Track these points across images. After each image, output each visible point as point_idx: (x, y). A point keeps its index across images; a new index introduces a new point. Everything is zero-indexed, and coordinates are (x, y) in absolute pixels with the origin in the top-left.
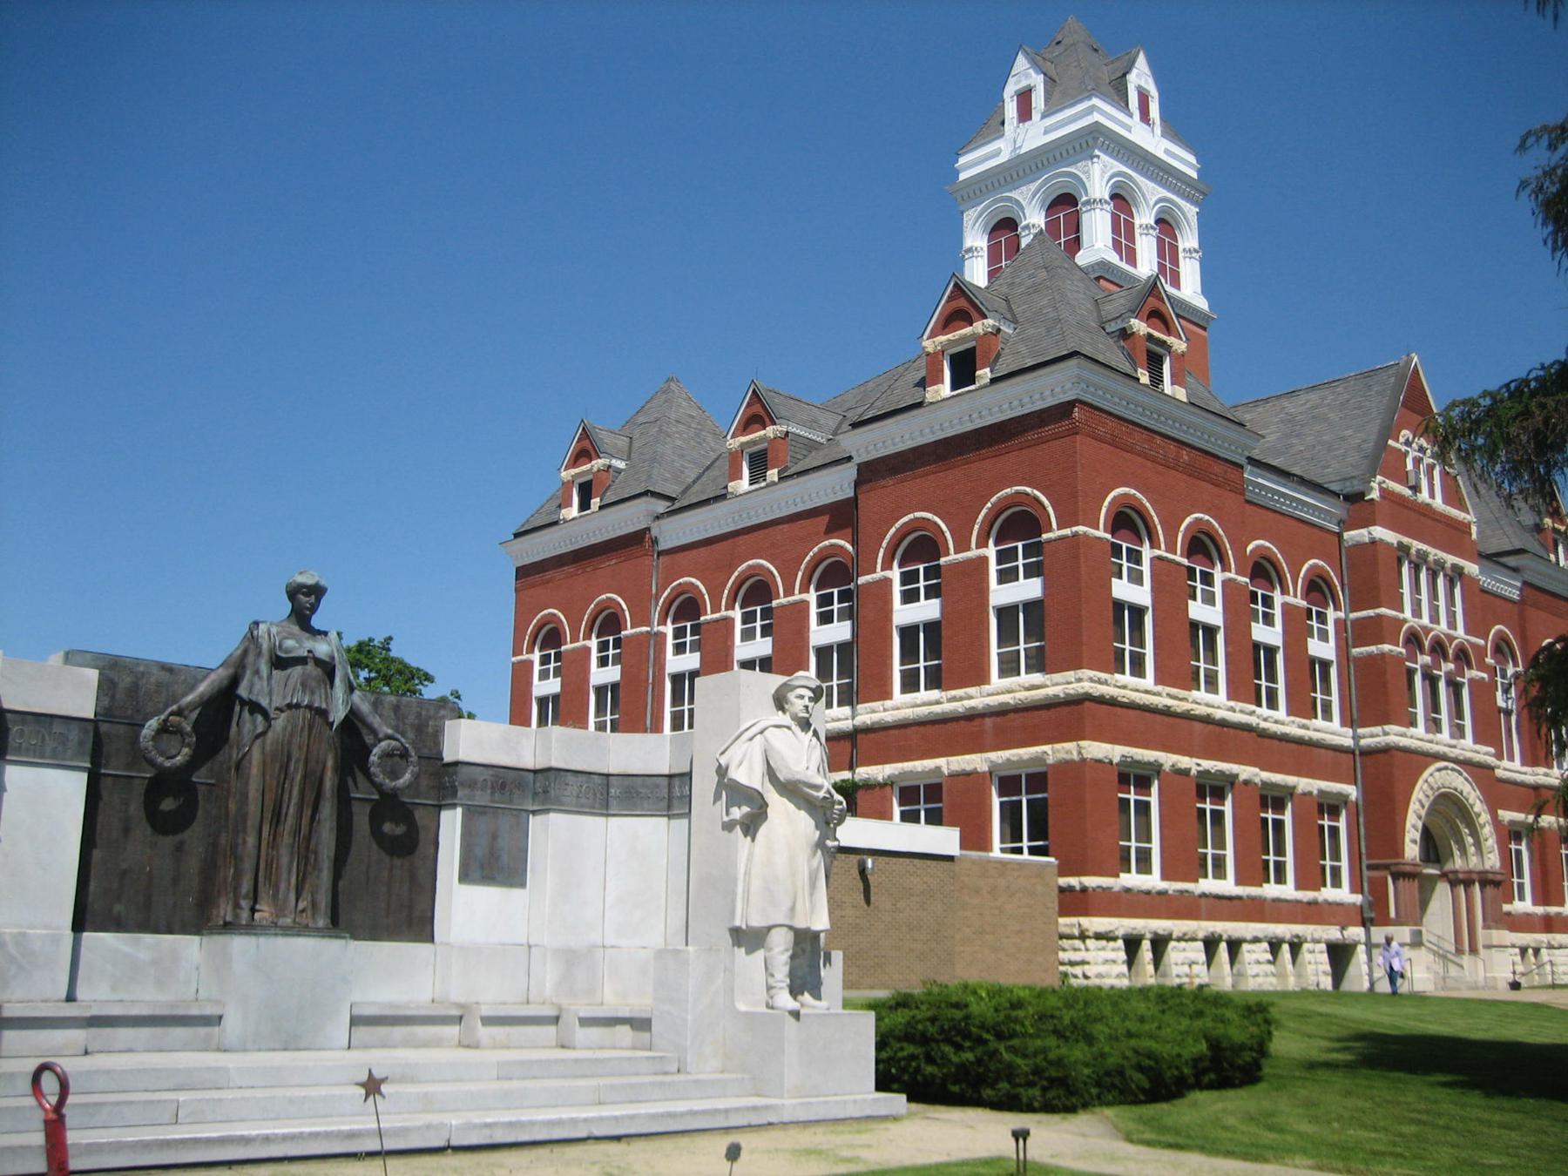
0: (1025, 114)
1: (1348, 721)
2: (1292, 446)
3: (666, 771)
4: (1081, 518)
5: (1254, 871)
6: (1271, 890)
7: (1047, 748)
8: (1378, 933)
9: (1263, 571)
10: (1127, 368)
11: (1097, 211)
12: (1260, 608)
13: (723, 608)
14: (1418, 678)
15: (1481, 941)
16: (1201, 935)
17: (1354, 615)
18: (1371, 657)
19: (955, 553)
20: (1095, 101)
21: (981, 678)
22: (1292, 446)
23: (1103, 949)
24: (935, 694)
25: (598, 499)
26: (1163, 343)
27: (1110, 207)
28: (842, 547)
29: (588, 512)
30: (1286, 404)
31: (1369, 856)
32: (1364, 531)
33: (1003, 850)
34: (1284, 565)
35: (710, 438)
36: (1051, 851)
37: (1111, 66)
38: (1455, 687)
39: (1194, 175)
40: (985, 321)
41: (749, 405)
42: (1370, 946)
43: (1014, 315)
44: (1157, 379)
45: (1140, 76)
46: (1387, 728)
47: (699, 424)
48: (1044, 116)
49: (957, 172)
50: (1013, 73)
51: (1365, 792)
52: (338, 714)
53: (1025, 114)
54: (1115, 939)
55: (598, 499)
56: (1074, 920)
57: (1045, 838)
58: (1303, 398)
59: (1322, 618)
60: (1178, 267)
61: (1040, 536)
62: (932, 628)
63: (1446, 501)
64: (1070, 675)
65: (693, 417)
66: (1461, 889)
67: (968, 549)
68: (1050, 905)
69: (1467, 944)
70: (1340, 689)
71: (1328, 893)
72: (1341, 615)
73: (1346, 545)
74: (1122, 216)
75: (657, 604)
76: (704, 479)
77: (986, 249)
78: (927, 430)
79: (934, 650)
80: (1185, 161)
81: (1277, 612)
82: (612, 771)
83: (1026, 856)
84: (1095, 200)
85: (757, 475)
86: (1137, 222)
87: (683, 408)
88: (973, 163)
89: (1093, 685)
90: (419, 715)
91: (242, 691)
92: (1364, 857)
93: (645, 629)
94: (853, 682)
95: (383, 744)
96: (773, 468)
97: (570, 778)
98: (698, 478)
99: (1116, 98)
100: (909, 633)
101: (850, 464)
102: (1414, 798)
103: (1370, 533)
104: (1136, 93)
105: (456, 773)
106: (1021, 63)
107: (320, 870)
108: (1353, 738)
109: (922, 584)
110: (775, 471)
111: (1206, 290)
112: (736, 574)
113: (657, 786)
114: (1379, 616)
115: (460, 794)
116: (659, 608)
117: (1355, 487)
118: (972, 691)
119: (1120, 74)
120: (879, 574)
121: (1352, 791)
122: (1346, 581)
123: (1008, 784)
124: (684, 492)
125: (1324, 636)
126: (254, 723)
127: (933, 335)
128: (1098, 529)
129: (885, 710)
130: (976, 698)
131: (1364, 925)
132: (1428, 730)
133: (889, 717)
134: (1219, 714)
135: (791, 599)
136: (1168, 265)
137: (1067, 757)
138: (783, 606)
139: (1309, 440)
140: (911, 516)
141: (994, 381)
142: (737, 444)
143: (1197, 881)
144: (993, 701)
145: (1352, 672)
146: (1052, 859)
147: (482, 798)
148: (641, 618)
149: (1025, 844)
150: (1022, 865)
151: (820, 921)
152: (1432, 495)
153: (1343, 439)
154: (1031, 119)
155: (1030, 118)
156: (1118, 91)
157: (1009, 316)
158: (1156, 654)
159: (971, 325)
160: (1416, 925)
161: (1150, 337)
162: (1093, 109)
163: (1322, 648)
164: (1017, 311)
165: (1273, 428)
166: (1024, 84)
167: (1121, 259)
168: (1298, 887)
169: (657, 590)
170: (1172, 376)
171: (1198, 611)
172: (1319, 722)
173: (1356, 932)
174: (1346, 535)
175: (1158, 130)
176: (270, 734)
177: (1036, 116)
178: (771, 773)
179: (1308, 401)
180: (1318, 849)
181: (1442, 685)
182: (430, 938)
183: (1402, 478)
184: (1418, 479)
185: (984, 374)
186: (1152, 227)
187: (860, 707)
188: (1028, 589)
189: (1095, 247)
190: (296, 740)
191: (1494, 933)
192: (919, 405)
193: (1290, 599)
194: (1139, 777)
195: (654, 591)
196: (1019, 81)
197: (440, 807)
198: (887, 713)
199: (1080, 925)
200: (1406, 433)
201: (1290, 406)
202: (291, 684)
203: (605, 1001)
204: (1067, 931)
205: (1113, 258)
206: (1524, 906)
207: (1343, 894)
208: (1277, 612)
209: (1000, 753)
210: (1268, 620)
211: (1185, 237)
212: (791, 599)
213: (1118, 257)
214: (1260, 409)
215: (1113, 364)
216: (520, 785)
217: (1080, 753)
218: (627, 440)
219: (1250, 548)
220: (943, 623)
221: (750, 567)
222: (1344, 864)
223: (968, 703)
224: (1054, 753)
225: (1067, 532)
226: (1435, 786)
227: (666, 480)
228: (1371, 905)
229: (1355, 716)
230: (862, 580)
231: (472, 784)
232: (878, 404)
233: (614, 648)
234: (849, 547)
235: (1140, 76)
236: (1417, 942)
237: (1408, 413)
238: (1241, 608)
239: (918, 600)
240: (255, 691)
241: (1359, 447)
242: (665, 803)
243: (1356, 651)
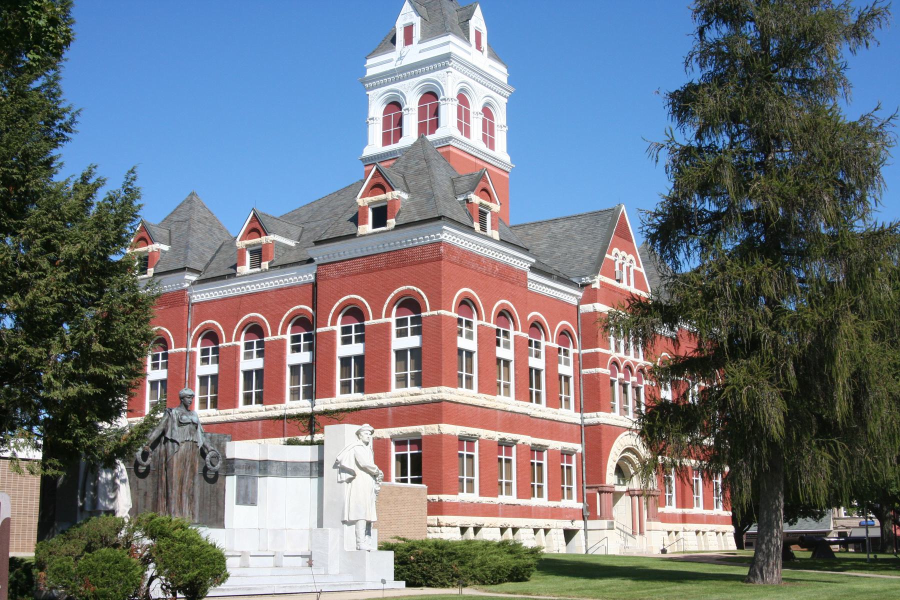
0: (408, 40)
1: (579, 409)
2: (554, 252)
5: (527, 491)
6: (535, 502)
7: (422, 427)
8: (591, 524)
9: (536, 326)
10: (468, 222)
11: (450, 105)
13: (233, 340)
14: (617, 384)
15: (645, 527)
16: (499, 525)
17: (583, 351)
19: (374, 319)
22: (554, 252)
24: (359, 395)
25: (152, 269)
26: (487, 207)
27: (457, 102)
29: (145, 276)
32: (591, 305)
33: (397, 481)
35: (217, 232)
37: (460, 12)
38: (638, 390)
39: (504, 79)
41: (250, 222)
42: (586, 530)
43: (408, 188)
44: (483, 228)
45: (477, 21)
46: (599, 413)
47: (210, 223)
48: (419, 43)
51: (587, 448)
52: (200, 445)
53: (408, 40)
54: (455, 526)
55: (152, 269)
56: (436, 517)
58: (561, 224)
59: (566, 353)
62: (359, 359)
63: (636, 287)
64: (436, 389)
65: (206, 218)
66: (636, 498)
67: (380, 317)
69: (638, 530)
70: (575, 393)
71: (565, 503)
72: (577, 351)
75: (191, 335)
76: (216, 259)
79: (361, 371)
80: (500, 72)
81: (543, 351)
83: (409, 484)
85: (256, 263)
86: (471, 110)
88: (376, 65)
90: (218, 440)
91: (168, 435)
92: (585, 483)
93: (184, 349)
94: (312, 386)
95: (210, 453)
97: (274, 464)
99: (463, 35)
100: (345, 361)
102: (612, 452)
106: (407, 7)
107: (195, 502)
111: (509, 150)
114: (597, 353)
116: (192, 337)
117: (584, 280)
118: (381, 395)
120: (329, 328)
122: (580, 332)
123: (401, 443)
126: (173, 447)
127: (363, 196)
128: (451, 311)
129: (332, 403)
131: (584, 519)
132: (621, 414)
133: (333, 407)
135: (276, 337)
137: (433, 432)
138: (271, 342)
139: (564, 250)
140: (348, 297)
141: (397, 227)
142: (243, 244)
144: (393, 401)
146: (424, 486)
149: (409, 477)
152: (629, 284)
153: (583, 251)
155: (411, 43)
158: (479, 377)
161: (481, 205)
163: (565, 369)
164: (410, 184)
166: (408, 21)
168: (481, 494)
172: (563, 410)
173: (579, 524)
174: (581, 307)
175: (486, 52)
176: (179, 452)
178: (357, 464)
180: (560, 480)
181: (630, 388)
182: (224, 527)
183: (612, 275)
185: (392, 223)
190: (188, 454)
191: (653, 523)
192: (354, 236)
193: (550, 344)
194: (470, 440)
195: (189, 327)
196: (405, 19)
201: (554, 228)
203: (305, 550)
205: (457, 134)
206: (671, 509)
207: (573, 503)
208: (543, 351)
209: (397, 429)
212: (276, 337)
213: (460, 133)
214: (537, 228)
216: (255, 467)
217: (439, 430)
221: (251, 317)
222: (574, 487)
223: (379, 402)
225: (435, 313)
227: (195, 260)
228: (588, 509)
229: (582, 407)
230: (319, 330)
231: (239, 467)
232: (330, 231)
234: (311, 310)
235: (477, 21)
238: (524, 348)
240: (174, 435)
241: (590, 258)
243: (585, 371)
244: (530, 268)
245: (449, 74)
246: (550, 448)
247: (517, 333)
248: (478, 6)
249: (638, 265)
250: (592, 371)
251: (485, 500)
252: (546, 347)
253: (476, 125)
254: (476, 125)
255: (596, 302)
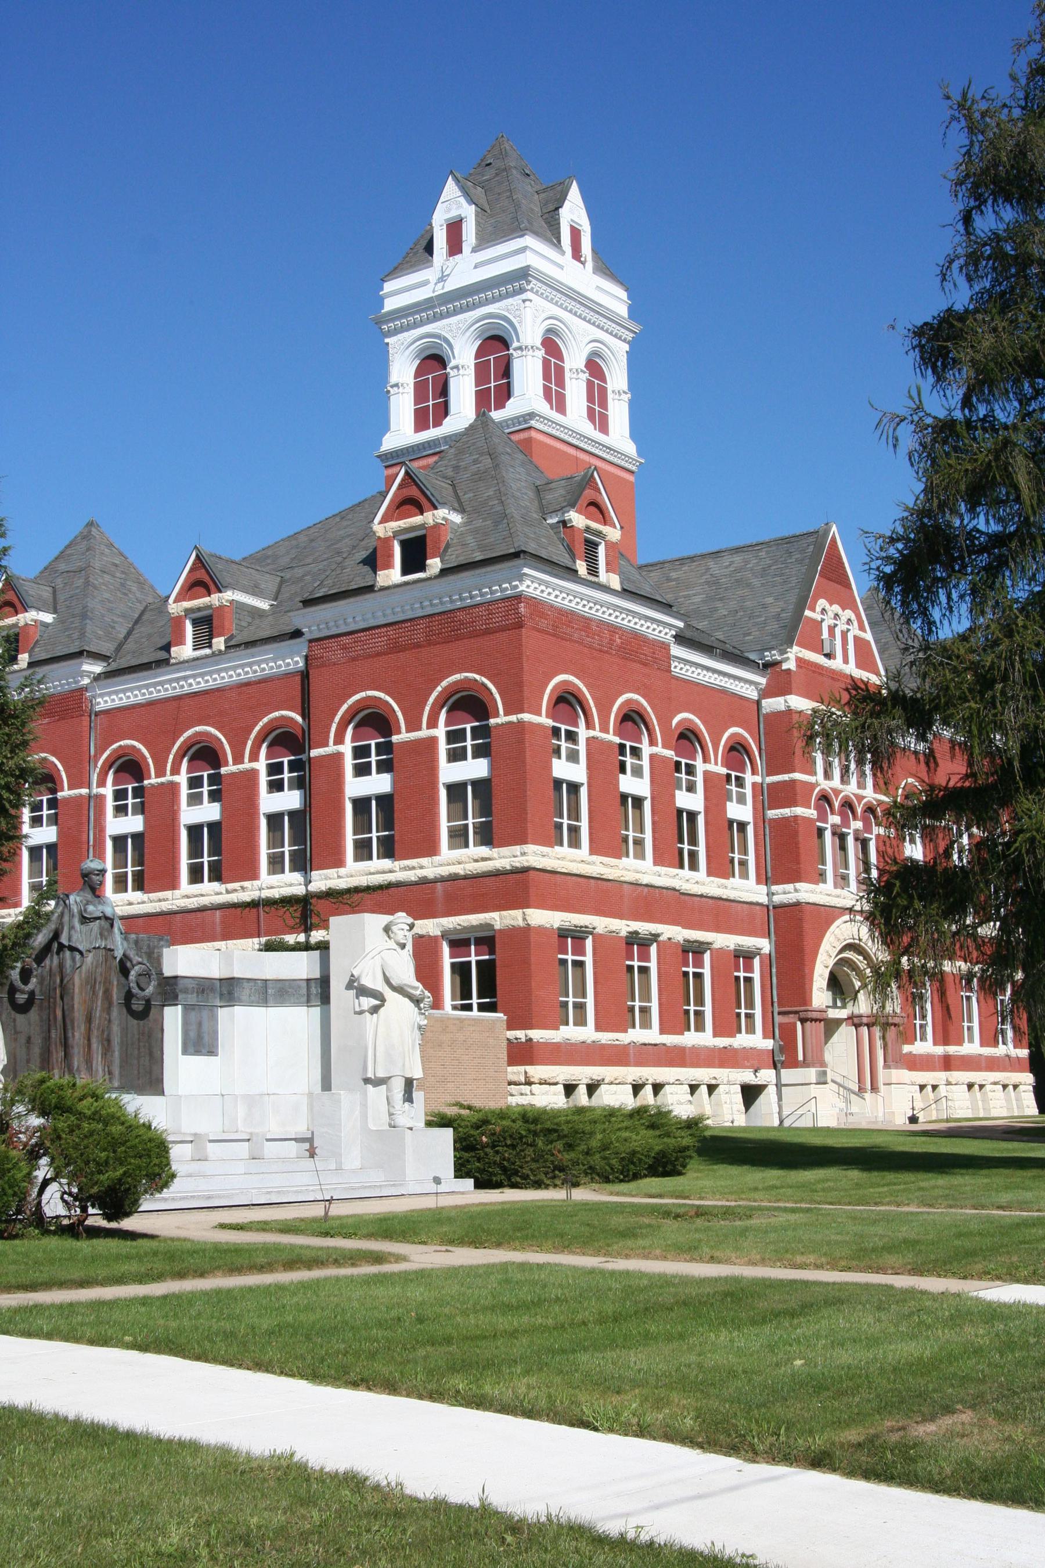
0: (455, 246)
1: (765, 878)
2: (716, 609)
3: (305, 977)
4: (526, 706)
8: (788, 1075)
12: (683, 776)
13: (168, 772)
14: (828, 835)
16: (630, 1080)
18: (785, 821)
19: (408, 731)
20: (529, 240)
21: (432, 850)
23: (546, 1093)
26: (599, 534)
27: (541, 353)
28: (292, 719)
30: (711, 564)
31: (779, 1005)
32: (780, 700)
34: (706, 735)
36: (499, 1007)
37: (543, 195)
38: (864, 843)
39: (623, 310)
40: (435, 512)
41: (192, 570)
42: (779, 1085)
44: (593, 570)
46: (798, 885)
47: (123, 572)
48: (474, 250)
49: (381, 301)
50: (442, 199)
51: (778, 946)
53: (455, 246)
54: (556, 1084)
56: (521, 1069)
57: (494, 996)
58: (726, 560)
59: (740, 782)
60: (607, 410)
61: (488, 719)
63: (859, 666)
65: (116, 565)
68: (500, 1056)
72: (758, 779)
73: (764, 712)
74: (553, 360)
75: (96, 766)
77: (412, 386)
78: (380, 614)
79: (387, 822)
81: (699, 780)
82: (268, 978)
83: (475, 1013)
84: (526, 347)
85: (203, 641)
87: (106, 556)
89: (536, 858)
90: (149, 946)
92: (776, 1005)
93: (84, 791)
95: (137, 968)
96: (219, 636)
98: (129, 633)
100: (361, 805)
101: (298, 640)
103: (786, 701)
104: (569, 228)
105: (176, 984)
106: (451, 189)
108: (768, 895)
109: (374, 759)
110: (222, 639)
111: (636, 433)
112: (182, 739)
113: (299, 987)
114: (793, 782)
115: (180, 997)
116: (98, 770)
118: (424, 861)
119: (552, 208)
120: (331, 749)
121: (764, 945)
122: (763, 747)
123: (459, 944)
124: (119, 648)
125: (742, 800)
126: (73, 959)
127: (384, 520)
129: (339, 877)
130: (428, 868)
134: (645, 880)
135: (241, 767)
136: (597, 408)
138: (232, 775)
139: (733, 604)
140: (363, 694)
141: (444, 572)
142: (180, 609)
143: (626, 1031)
144: (445, 871)
145: (767, 832)
147: (192, 999)
148: (79, 780)
149: (475, 1001)
150: (475, 1020)
151: (417, 1073)
152: (846, 661)
153: (764, 606)
154: (461, 252)
156: (550, 231)
157: (456, 505)
159: (422, 513)
160: (821, 1066)
161: (588, 529)
162: (523, 250)
163: (740, 811)
165: (698, 589)
166: (454, 213)
167: (552, 408)
169: (96, 751)
170: (607, 564)
171: (628, 784)
173: (767, 1075)
174: (765, 703)
175: (590, 264)
176: (84, 968)
177: (466, 248)
179: (732, 563)
181: (850, 841)
182: (162, 1093)
183: (817, 646)
184: (833, 646)
185: (434, 564)
186: (582, 371)
187: (315, 874)
188: (476, 768)
189: (527, 396)
191: (894, 1071)
192: (370, 589)
193: (711, 767)
194: (577, 936)
196: (449, 210)
197: (164, 1006)
198: (341, 880)
199: (526, 1073)
200: (822, 603)
202: (93, 934)
204: (514, 1078)
207: (757, 1040)
208: (699, 780)
209: (452, 919)
210: (691, 788)
211: (614, 375)
212: (241, 767)
214: (686, 568)
215: (555, 559)
216: (212, 990)
217: (524, 919)
218: (50, 589)
219: (675, 722)
220: (395, 797)
224: (501, 919)
225: (513, 718)
226: (842, 938)
227: (99, 638)
228: (782, 1049)
229: (769, 875)
230: (314, 753)
231: (186, 991)
232: (329, 582)
233: (49, 809)
234: (299, 719)
236: (822, 1081)
237: (825, 581)
239: (369, 773)
241: (777, 617)
242: (305, 999)
243: (772, 814)
244: (675, 637)
245: (527, 303)
246: (716, 946)
247: (655, 750)
248: (451, 183)
249: (862, 628)
250: (786, 812)
251: (606, 1037)
252: (706, 773)
253: (576, 391)
254: (576, 391)
255: (790, 693)
